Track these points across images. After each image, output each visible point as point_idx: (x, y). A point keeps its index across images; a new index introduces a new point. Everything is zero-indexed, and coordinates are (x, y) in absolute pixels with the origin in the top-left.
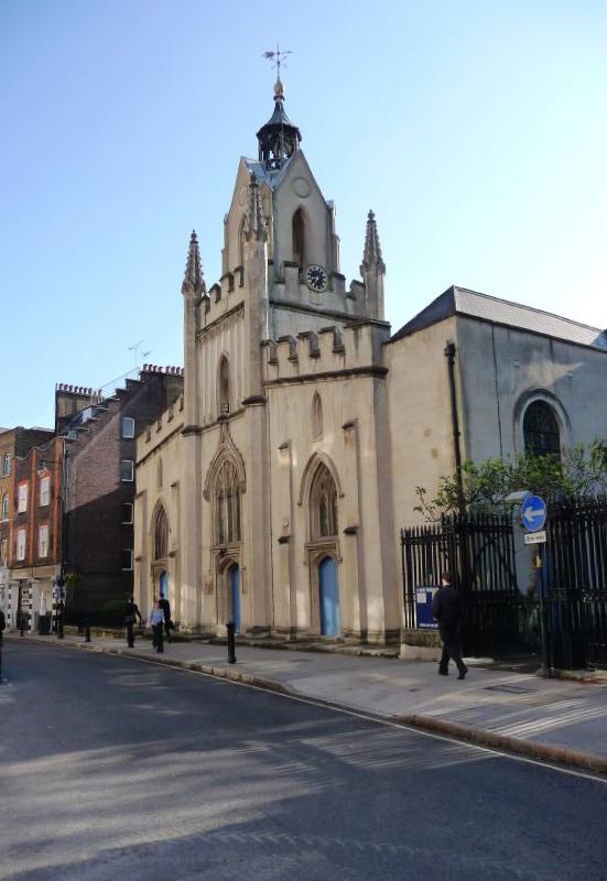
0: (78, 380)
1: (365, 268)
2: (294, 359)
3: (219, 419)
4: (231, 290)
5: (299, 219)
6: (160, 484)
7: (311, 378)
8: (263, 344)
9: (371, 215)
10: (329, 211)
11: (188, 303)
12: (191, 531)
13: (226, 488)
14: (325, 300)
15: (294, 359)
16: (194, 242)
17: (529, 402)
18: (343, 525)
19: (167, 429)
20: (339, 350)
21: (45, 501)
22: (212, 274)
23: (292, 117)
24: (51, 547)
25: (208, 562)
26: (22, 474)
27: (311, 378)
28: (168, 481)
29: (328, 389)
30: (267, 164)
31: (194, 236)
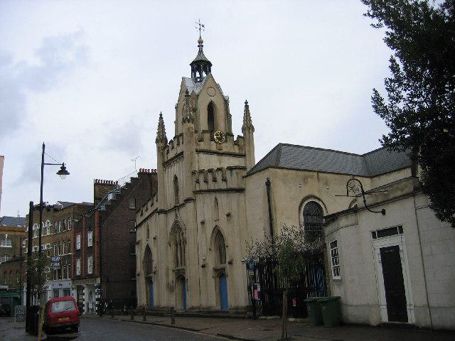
0: (105, 177)
1: (243, 129)
2: (206, 182)
3: (175, 207)
4: (178, 144)
5: (211, 107)
6: (148, 237)
7: (215, 191)
8: (193, 173)
9: (246, 103)
10: (226, 102)
11: (158, 148)
12: (163, 259)
13: (178, 237)
14: (226, 147)
15: (206, 182)
16: (161, 118)
17: (306, 203)
18: (228, 260)
19: (150, 210)
20: (224, 180)
21: (90, 244)
22: (170, 135)
23: (208, 55)
24: (94, 268)
25: (172, 277)
26: (78, 229)
27: (215, 191)
28: (152, 236)
29: (223, 198)
30: (195, 79)
31: (161, 115)
